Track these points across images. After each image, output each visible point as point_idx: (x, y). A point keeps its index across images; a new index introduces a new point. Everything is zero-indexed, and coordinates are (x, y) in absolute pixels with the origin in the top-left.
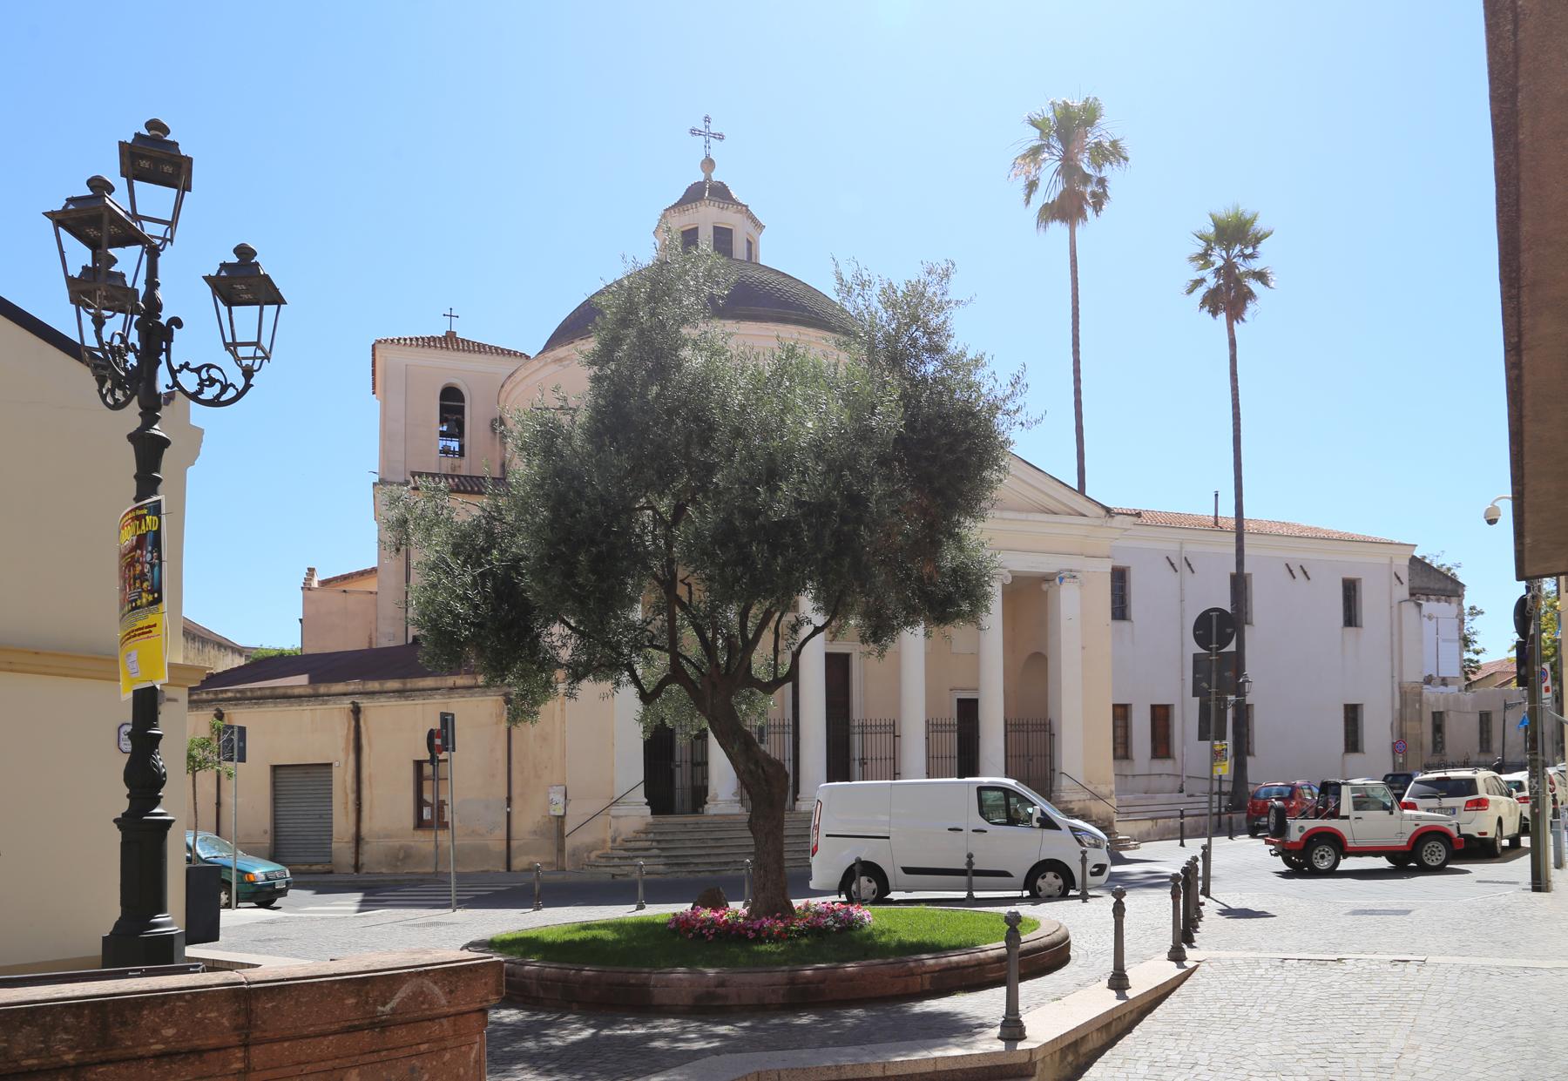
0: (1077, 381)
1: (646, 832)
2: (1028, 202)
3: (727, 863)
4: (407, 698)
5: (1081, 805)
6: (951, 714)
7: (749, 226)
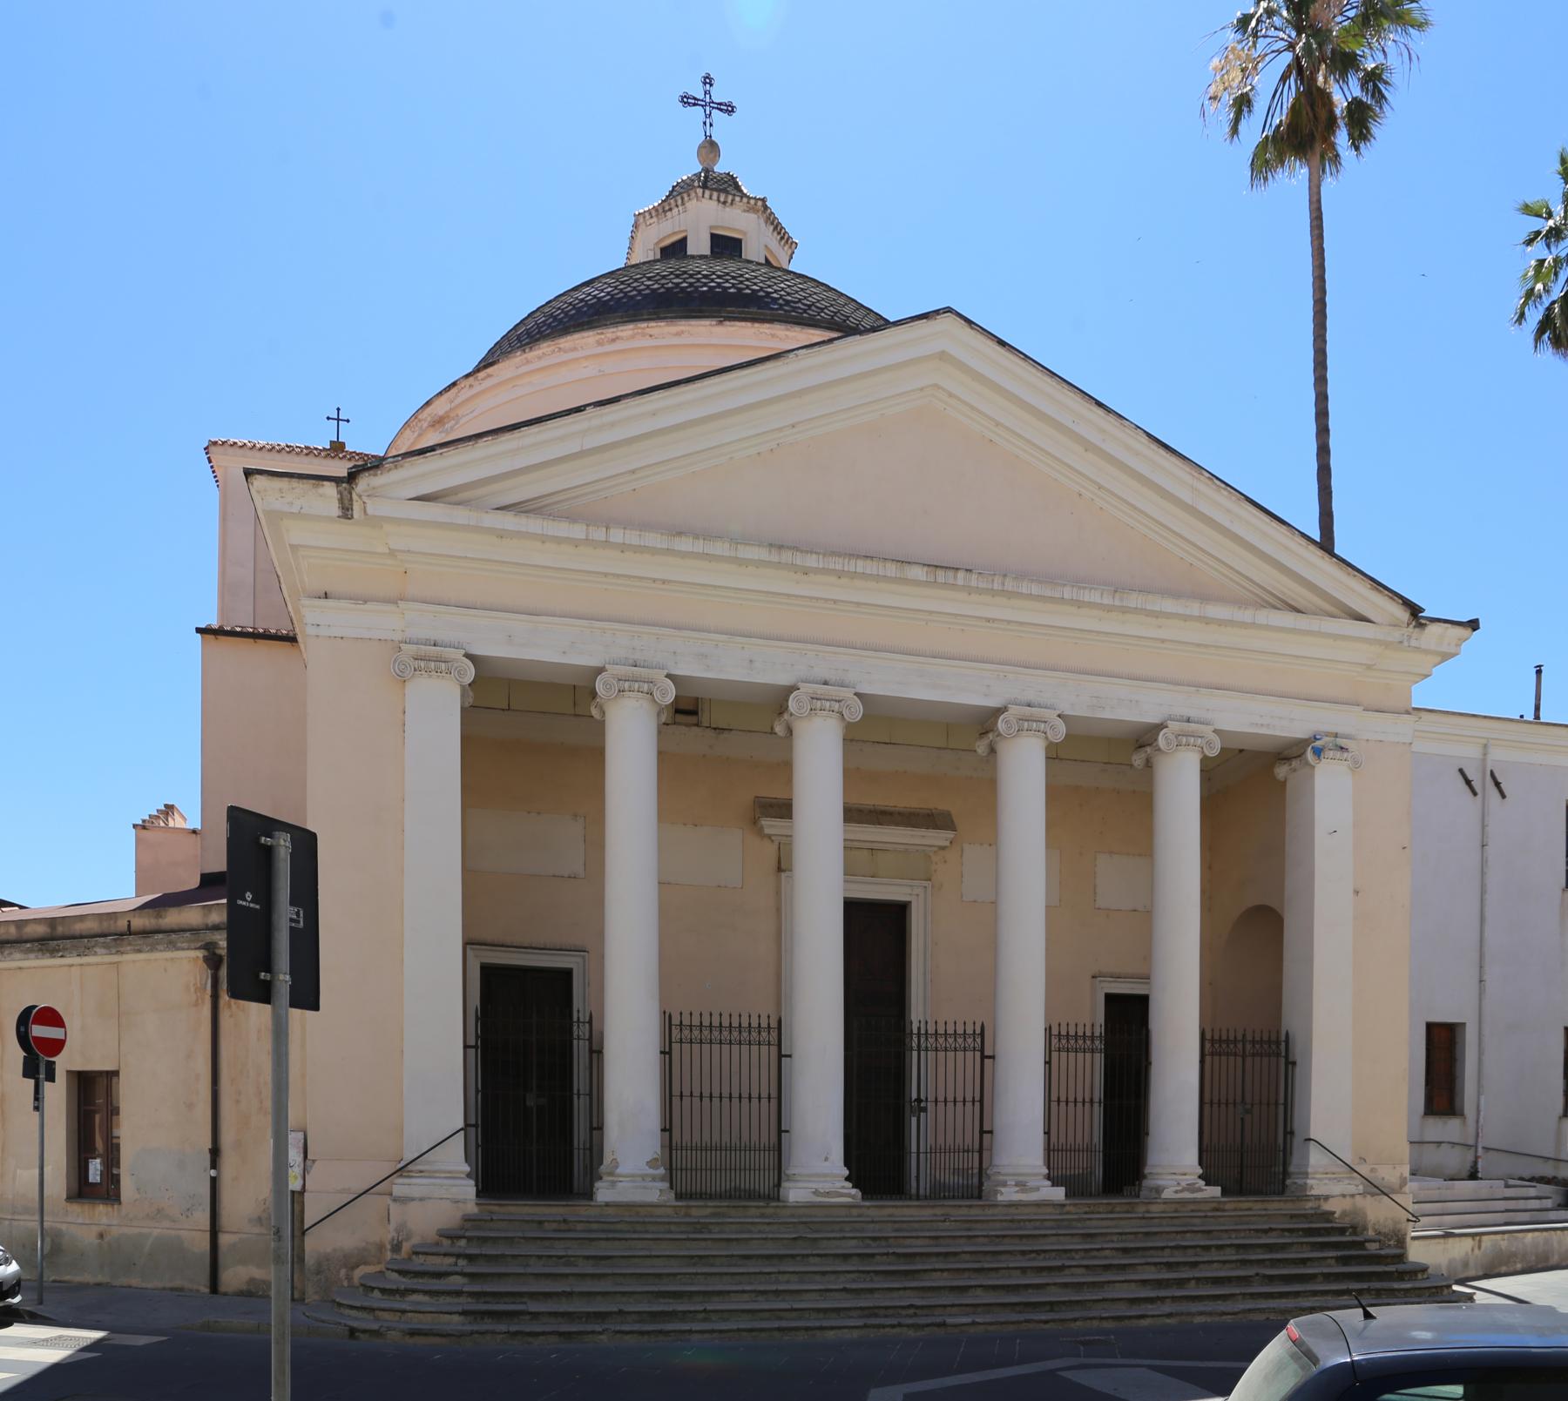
0: (1323, 431)
1: (452, 1237)
2: (1235, 130)
3: (601, 1316)
4: (53, 952)
5: (1346, 1204)
6: (1093, 1017)
7: (772, 240)
